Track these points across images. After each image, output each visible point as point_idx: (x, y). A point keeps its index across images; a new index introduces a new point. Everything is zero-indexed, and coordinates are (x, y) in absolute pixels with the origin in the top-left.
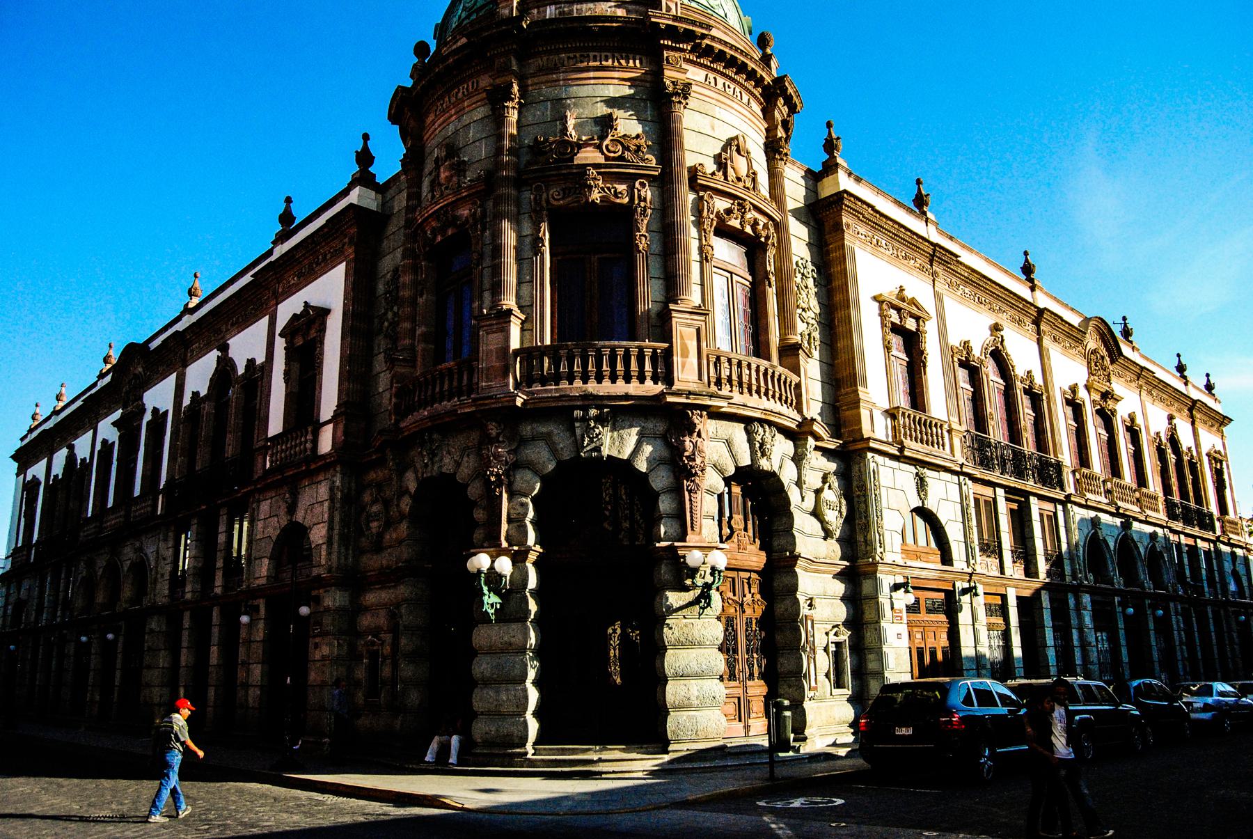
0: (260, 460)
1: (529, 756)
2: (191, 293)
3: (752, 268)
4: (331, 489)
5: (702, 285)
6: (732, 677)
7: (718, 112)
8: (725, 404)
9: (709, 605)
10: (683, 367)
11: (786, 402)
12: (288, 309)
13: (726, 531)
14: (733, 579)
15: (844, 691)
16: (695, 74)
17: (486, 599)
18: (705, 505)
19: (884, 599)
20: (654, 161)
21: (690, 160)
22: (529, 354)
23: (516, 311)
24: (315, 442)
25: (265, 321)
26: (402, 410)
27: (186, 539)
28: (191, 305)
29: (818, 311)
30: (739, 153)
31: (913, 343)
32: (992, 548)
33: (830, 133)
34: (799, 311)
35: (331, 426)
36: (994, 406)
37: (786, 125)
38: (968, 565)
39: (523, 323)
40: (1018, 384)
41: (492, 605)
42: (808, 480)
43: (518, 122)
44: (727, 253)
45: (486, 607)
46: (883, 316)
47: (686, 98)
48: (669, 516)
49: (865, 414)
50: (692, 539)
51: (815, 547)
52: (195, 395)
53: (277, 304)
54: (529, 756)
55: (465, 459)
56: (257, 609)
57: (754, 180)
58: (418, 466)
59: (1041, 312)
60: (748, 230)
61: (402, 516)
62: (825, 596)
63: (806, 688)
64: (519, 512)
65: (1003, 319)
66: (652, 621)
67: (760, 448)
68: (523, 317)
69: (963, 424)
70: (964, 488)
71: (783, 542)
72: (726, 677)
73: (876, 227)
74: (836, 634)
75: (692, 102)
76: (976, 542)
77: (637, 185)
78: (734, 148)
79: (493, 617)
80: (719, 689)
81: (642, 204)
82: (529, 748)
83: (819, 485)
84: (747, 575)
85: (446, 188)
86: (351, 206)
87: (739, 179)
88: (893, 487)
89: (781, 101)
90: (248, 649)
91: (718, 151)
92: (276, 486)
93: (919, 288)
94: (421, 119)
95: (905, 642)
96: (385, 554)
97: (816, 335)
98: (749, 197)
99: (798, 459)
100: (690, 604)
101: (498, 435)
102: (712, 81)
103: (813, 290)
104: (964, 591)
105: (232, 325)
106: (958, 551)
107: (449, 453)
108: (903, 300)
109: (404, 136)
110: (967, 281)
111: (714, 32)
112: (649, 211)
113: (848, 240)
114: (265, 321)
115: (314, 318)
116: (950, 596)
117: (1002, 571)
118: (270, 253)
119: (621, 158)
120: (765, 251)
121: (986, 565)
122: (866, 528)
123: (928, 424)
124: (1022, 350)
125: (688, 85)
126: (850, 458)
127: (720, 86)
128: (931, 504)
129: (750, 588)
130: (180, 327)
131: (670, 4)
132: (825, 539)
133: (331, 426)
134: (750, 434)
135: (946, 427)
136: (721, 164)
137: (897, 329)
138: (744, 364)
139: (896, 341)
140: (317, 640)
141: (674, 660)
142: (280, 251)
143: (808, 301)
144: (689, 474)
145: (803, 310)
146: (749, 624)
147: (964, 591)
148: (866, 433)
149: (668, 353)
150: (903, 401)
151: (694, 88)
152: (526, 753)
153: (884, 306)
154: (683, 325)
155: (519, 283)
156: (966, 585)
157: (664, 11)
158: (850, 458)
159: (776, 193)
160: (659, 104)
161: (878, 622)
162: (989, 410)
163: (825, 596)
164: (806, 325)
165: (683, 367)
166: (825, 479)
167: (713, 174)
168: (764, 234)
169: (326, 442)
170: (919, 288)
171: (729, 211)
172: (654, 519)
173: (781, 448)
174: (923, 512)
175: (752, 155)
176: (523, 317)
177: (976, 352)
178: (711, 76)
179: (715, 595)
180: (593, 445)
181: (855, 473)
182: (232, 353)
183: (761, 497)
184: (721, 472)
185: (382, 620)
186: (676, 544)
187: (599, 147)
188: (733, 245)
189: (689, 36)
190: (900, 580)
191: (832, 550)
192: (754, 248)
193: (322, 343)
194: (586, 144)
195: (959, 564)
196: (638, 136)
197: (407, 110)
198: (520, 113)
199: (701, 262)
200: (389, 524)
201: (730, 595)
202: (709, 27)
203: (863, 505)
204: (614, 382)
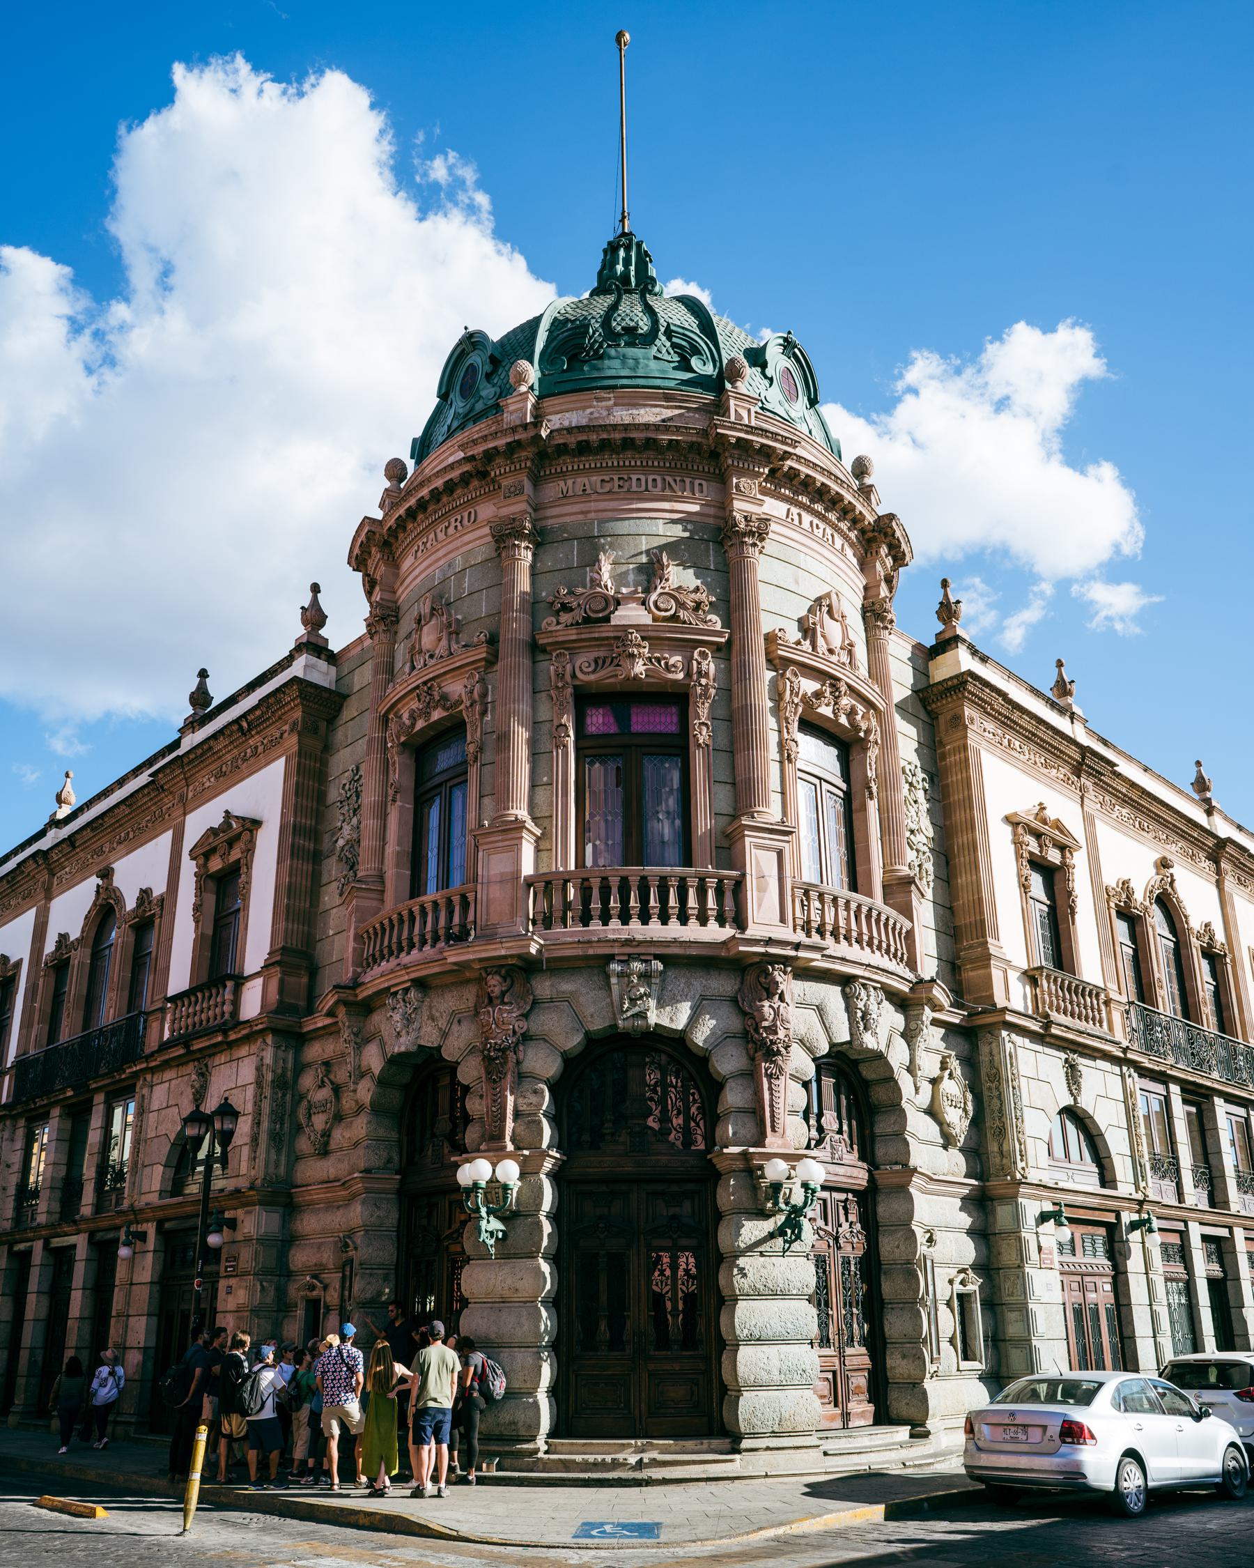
0: (155, 1025)
1: (541, 1455)
2: (60, 800)
3: (846, 775)
4: (258, 1069)
5: (783, 793)
6: (825, 1341)
7: (802, 560)
8: (818, 956)
9: (798, 1237)
10: (760, 905)
11: (895, 956)
12: (201, 821)
13: (814, 1134)
14: (825, 1201)
15: (975, 1365)
16: (774, 507)
17: (483, 1224)
18: (788, 1098)
19: (1028, 1235)
20: (719, 622)
21: (767, 624)
22: (546, 884)
23: (530, 824)
24: (236, 1003)
25: (167, 837)
26: (366, 961)
27: (125, 1113)
28: (61, 815)
29: (931, 834)
30: (832, 617)
31: (1054, 877)
32: (1168, 1167)
33: (946, 595)
34: (908, 834)
35: (259, 982)
36: (1162, 970)
37: (889, 580)
38: (1137, 1189)
39: (538, 840)
40: (1194, 940)
41: (492, 1233)
42: (923, 1070)
43: (533, 567)
44: (816, 755)
45: (484, 1236)
46: (1018, 844)
47: (762, 540)
48: (741, 1111)
49: (997, 975)
50: (773, 1143)
51: (934, 1158)
52: (63, 937)
53: (185, 814)
54: (541, 1455)
55: (455, 1027)
56: (142, 1237)
57: (850, 653)
58: (385, 1034)
59: (1222, 843)
60: (843, 720)
61: (360, 1109)
62: (948, 1228)
63: (928, 1359)
64: (527, 1108)
65: (1173, 850)
66: (715, 1261)
67: (863, 1018)
68: (538, 832)
69: (1122, 992)
70: (1129, 1081)
71: (892, 1151)
72: (816, 1342)
73: (1007, 723)
74: (963, 1283)
75: (769, 546)
76: (1146, 1157)
77: (696, 655)
78: (825, 609)
79: (493, 1251)
80: (810, 1359)
81: (703, 681)
82: (541, 1443)
83: (936, 1072)
84: (843, 1196)
85: (431, 656)
86: (295, 680)
87: (831, 651)
88: (1035, 1077)
89: (884, 550)
90: (128, 1295)
91: (804, 613)
92: (178, 1062)
93: (1064, 807)
94: (394, 562)
95: (1057, 1296)
96: (332, 1158)
97: (929, 866)
98: (845, 676)
99: (909, 1035)
100: (771, 1236)
101: (503, 994)
102: (796, 518)
103: (924, 806)
104: (1134, 1226)
105: (120, 843)
106: (1122, 1169)
107: (432, 1018)
108: (1044, 822)
109: (370, 586)
110: (1126, 801)
111: (799, 451)
112: (713, 692)
113: (973, 739)
114: (167, 837)
115: (238, 832)
116: (1112, 1230)
117: (1180, 1195)
118: (176, 744)
119: (674, 618)
120: (866, 749)
121: (1159, 1190)
122: (1002, 1132)
123: (1082, 990)
124: (1198, 896)
125: (765, 521)
126: (975, 1037)
127: (806, 525)
128: (1086, 1102)
129: (846, 1214)
130: (44, 844)
131: (741, 411)
132: (945, 1147)
133: (259, 982)
134: (847, 997)
135: (1102, 996)
136: (807, 631)
137: (1038, 864)
138: (841, 902)
139: (1036, 881)
140: (233, 1281)
141: (748, 1315)
142: (189, 741)
143: (918, 819)
144: (770, 1053)
145: (912, 832)
146: (846, 1262)
147: (1134, 1226)
148: (1000, 1002)
149: (739, 884)
150: (1040, 958)
151: (773, 527)
152: (537, 1451)
153: (1020, 830)
154: (758, 847)
155: (533, 786)
156: (1135, 1217)
157: (733, 419)
158: (975, 1037)
159: (877, 672)
160: (722, 548)
161: (1020, 1267)
162: (1157, 975)
163: (948, 1228)
164: (917, 857)
165: (760, 905)
166: (944, 1066)
167: (798, 643)
168: (864, 726)
169: (252, 1003)
170: (1064, 807)
171: (818, 695)
172: (713, 1118)
173: (888, 1019)
174: (1074, 1115)
175: (848, 621)
176: (538, 832)
177: (1139, 896)
178: (795, 510)
179: (807, 1226)
180: (637, 1009)
181: (984, 1058)
182: (118, 881)
183: (857, 1086)
184: (810, 1050)
185: (328, 1257)
186: (752, 1150)
187: (644, 603)
188: (820, 743)
189: (766, 454)
190: (1048, 1207)
191: (953, 1164)
192: (847, 745)
193: (249, 867)
194: (630, 598)
195: (1125, 1188)
196: (697, 589)
197: (376, 549)
198: (534, 555)
199: (781, 762)
200: (338, 1118)
201: (821, 1223)
202: (794, 444)
203: (996, 1102)
204: (665, 923)
